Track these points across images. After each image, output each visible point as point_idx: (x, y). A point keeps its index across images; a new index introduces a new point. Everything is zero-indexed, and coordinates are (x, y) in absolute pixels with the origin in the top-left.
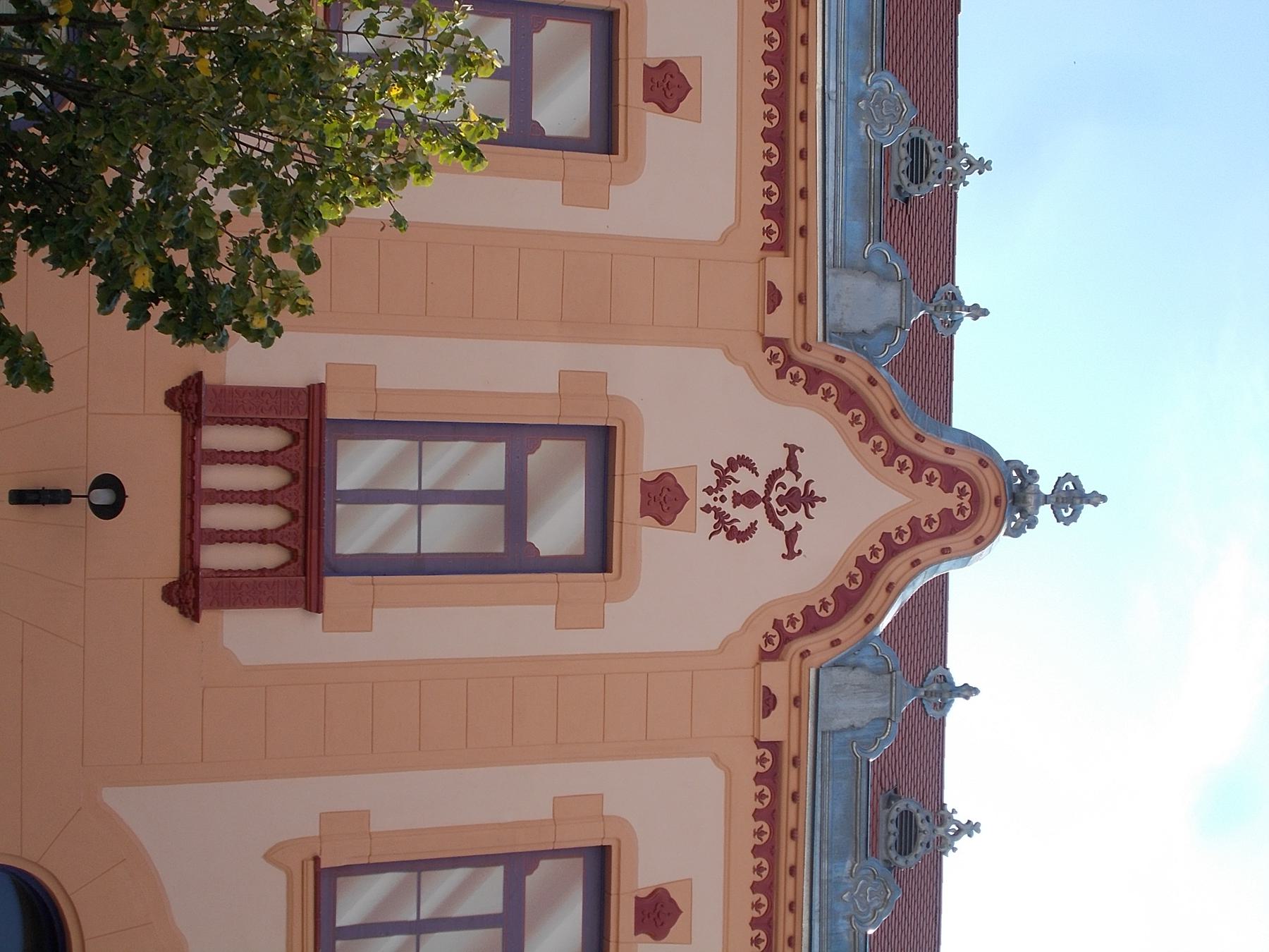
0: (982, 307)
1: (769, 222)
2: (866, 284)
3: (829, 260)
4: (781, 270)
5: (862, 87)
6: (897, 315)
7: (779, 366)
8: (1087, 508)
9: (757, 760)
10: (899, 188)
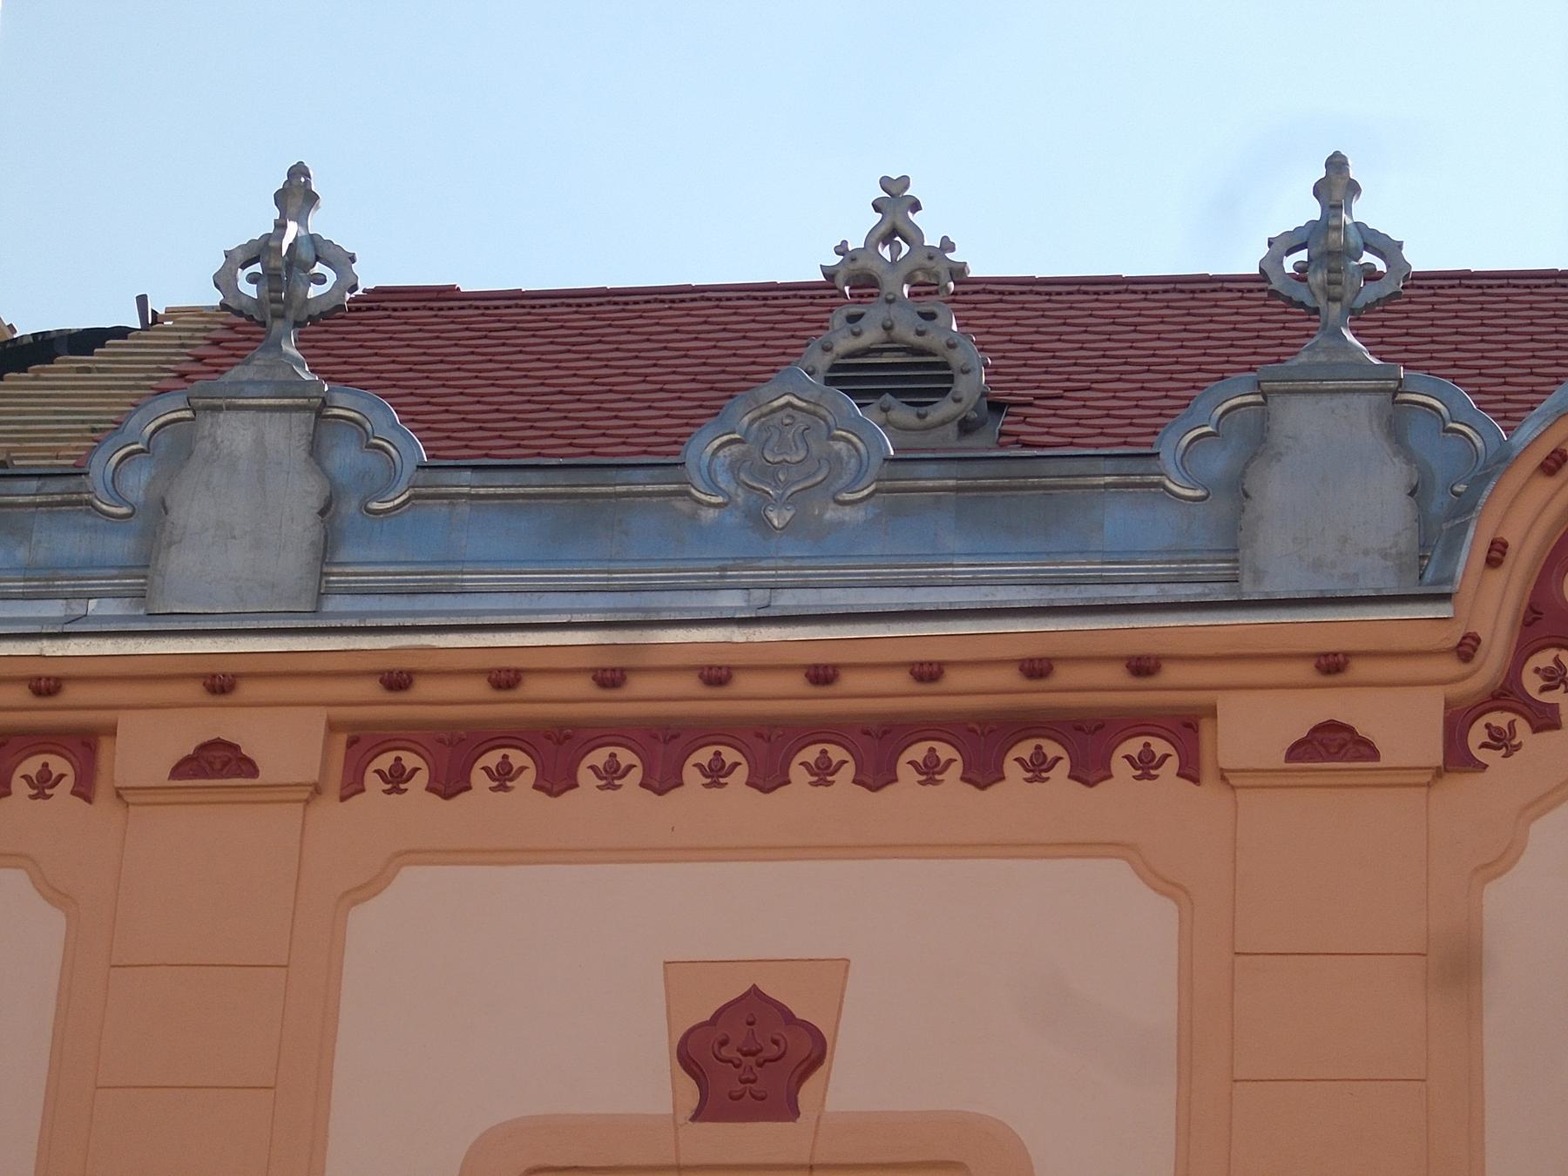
0: (1321, 173)
1: (1119, 765)
2: (1275, 489)
3: (1219, 593)
4: (1255, 728)
5: (732, 519)
6: (1361, 402)
7: (1522, 726)
8: (1363, 211)
9: (1146, 776)
10: (966, 427)
